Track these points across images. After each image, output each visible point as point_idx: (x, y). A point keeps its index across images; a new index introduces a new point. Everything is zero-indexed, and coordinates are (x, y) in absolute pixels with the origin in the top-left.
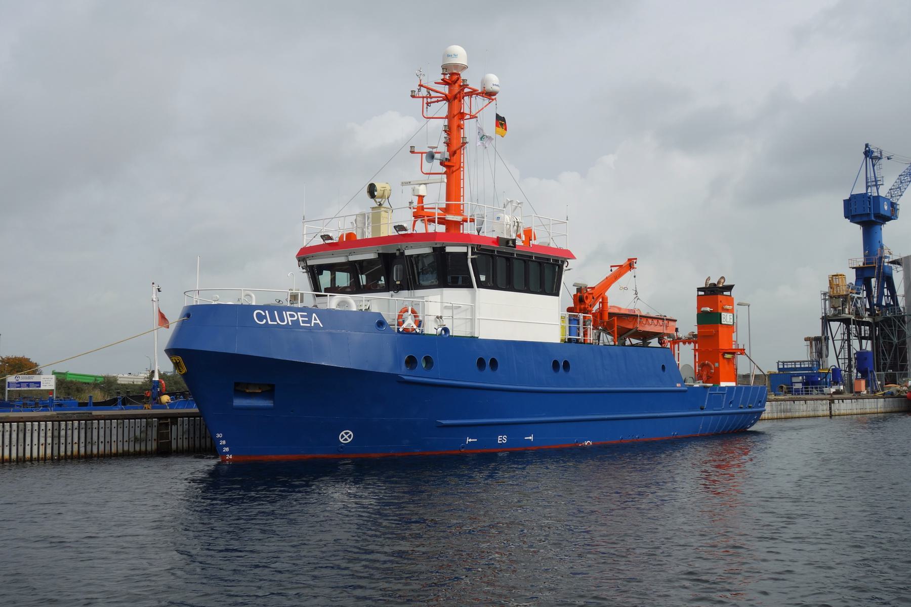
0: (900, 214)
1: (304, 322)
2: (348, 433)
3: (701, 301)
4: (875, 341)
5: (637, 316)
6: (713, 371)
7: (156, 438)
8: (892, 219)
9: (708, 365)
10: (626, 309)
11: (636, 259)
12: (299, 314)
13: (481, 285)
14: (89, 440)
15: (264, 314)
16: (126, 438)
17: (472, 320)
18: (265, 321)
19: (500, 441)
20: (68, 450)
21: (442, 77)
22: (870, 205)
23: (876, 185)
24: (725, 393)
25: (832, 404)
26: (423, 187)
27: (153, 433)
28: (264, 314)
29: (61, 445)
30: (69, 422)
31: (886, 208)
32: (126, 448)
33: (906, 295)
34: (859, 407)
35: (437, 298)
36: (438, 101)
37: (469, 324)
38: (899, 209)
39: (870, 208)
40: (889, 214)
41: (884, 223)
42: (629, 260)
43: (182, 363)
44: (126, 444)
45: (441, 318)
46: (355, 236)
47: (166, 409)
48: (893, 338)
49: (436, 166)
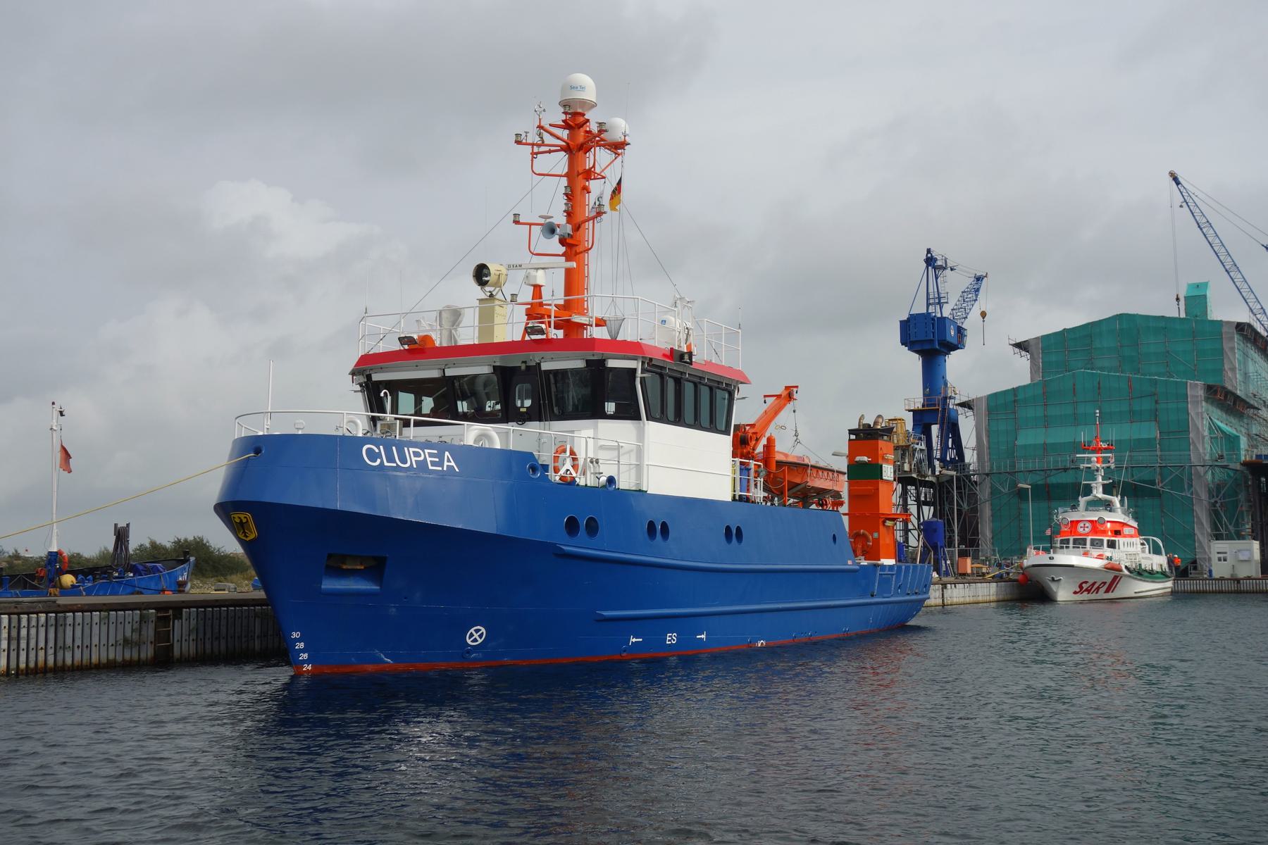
0: (968, 341)
1: (433, 463)
2: (479, 630)
3: (854, 448)
4: (938, 508)
5: (808, 466)
6: (871, 544)
7: (153, 640)
8: (958, 348)
9: (864, 536)
10: (794, 457)
11: (797, 387)
12: (427, 451)
13: (650, 417)
14: (60, 643)
15: (377, 451)
16: (112, 641)
17: (639, 467)
18: (379, 461)
19: (669, 641)
20: (30, 659)
21: (564, 117)
22: (933, 328)
23: (939, 303)
24: (893, 574)
26: (541, 272)
27: (149, 632)
28: (377, 451)
29: (21, 652)
30: (51, 615)
31: (952, 333)
32: (111, 656)
33: (979, 448)
34: (971, 595)
35: (589, 433)
36: (550, 152)
37: (633, 472)
38: (966, 336)
39: (933, 333)
40: (955, 341)
41: (949, 354)
42: (787, 388)
43: (252, 525)
44: (112, 649)
45: (597, 463)
46: (433, 341)
47: (81, 595)
48: (962, 503)
49: (554, 245)
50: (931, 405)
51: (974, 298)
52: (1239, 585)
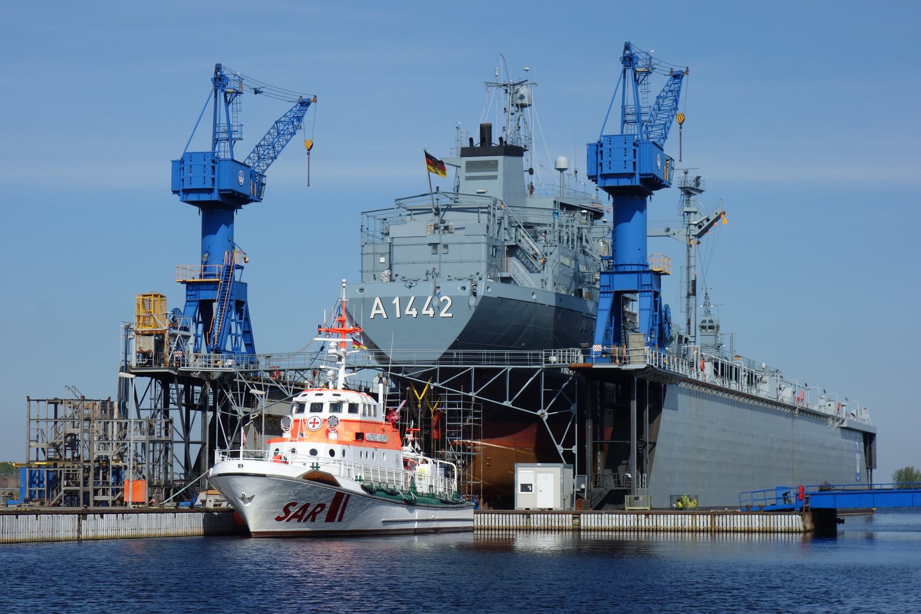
0: (267, 192)
8: (252, 201)
25: (83, 521)
38: (265, 184)
50: (206, 276)
52: (528, 520)
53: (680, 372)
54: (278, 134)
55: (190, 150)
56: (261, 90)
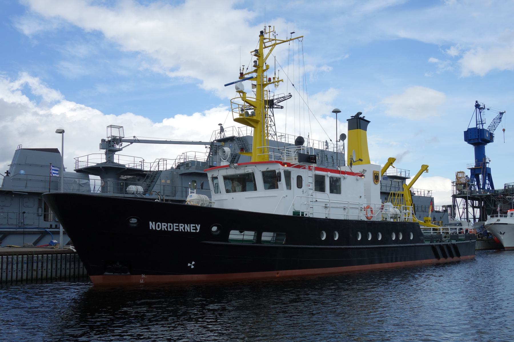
0: (495, 139)
31: (487, 135)
41: (486, 144)
50: (478, 166)
51: (499, 121)
53: (169, 230)
54: (495, 123)
55: (470, 127)
56: (489, 109)
